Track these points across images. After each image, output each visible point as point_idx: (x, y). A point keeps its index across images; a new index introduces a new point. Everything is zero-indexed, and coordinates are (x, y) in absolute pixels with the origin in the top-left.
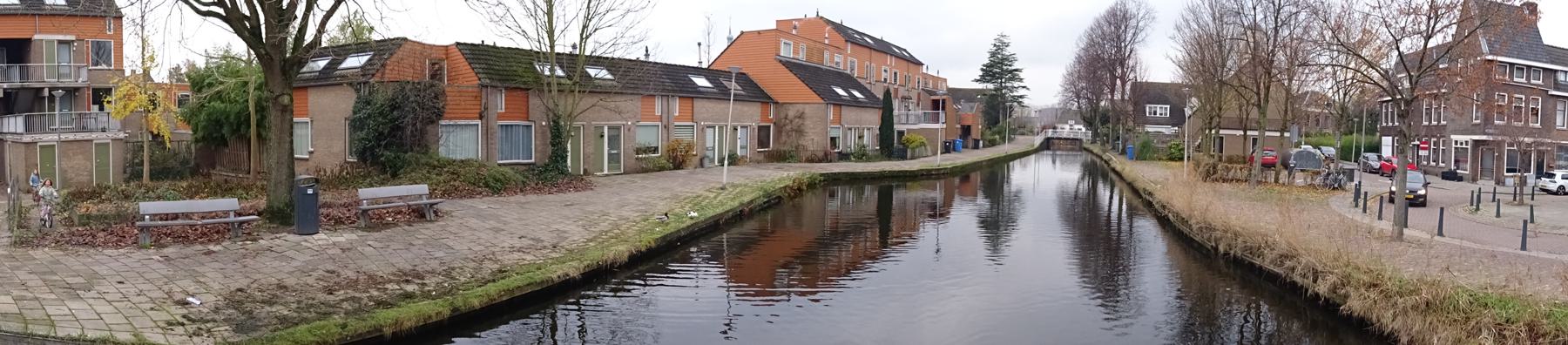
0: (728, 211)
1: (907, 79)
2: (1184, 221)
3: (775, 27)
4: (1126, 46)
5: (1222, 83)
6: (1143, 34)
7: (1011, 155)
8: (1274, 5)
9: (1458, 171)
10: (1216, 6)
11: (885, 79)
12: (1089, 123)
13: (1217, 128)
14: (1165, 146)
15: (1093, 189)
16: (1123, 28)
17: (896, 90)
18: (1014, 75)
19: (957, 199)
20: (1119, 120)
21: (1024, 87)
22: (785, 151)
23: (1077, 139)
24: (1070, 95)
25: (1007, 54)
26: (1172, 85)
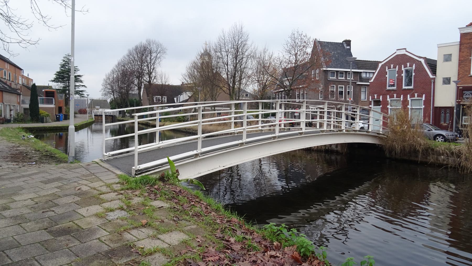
21: (83, 86)
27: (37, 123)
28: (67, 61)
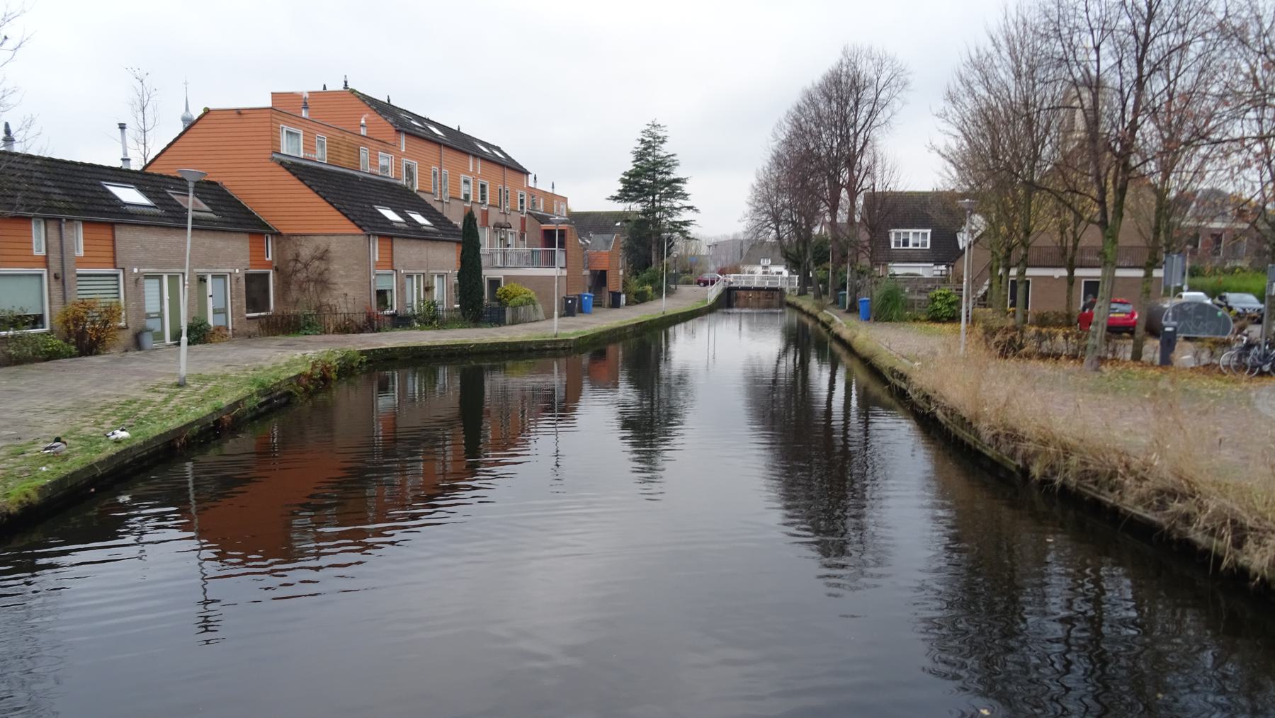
0: (191, 424)
1: (503, 195)
2: (965, 423)
3: (269, 104)
4: (856, 135)
5: (1031, 186)
6: (887, 111)
7: (671, 316)
8: (1137, 37)
10: (1022, 53)
11: (467, 197)
12: (794, 262)
13: (1021, 267)
14: (924, 297)
15: (802, 368)
16: (852, 103)
17: (485, 214)
18: (673, 188)
19: (586, 387)
20: (845, 256)
21: (689, 208)
22: (297, 317)
23: (776, 289)
24: (764, 217)
25: (662, 154)
26: (937, 196)
27: (476, 327)
28: (649, 141)
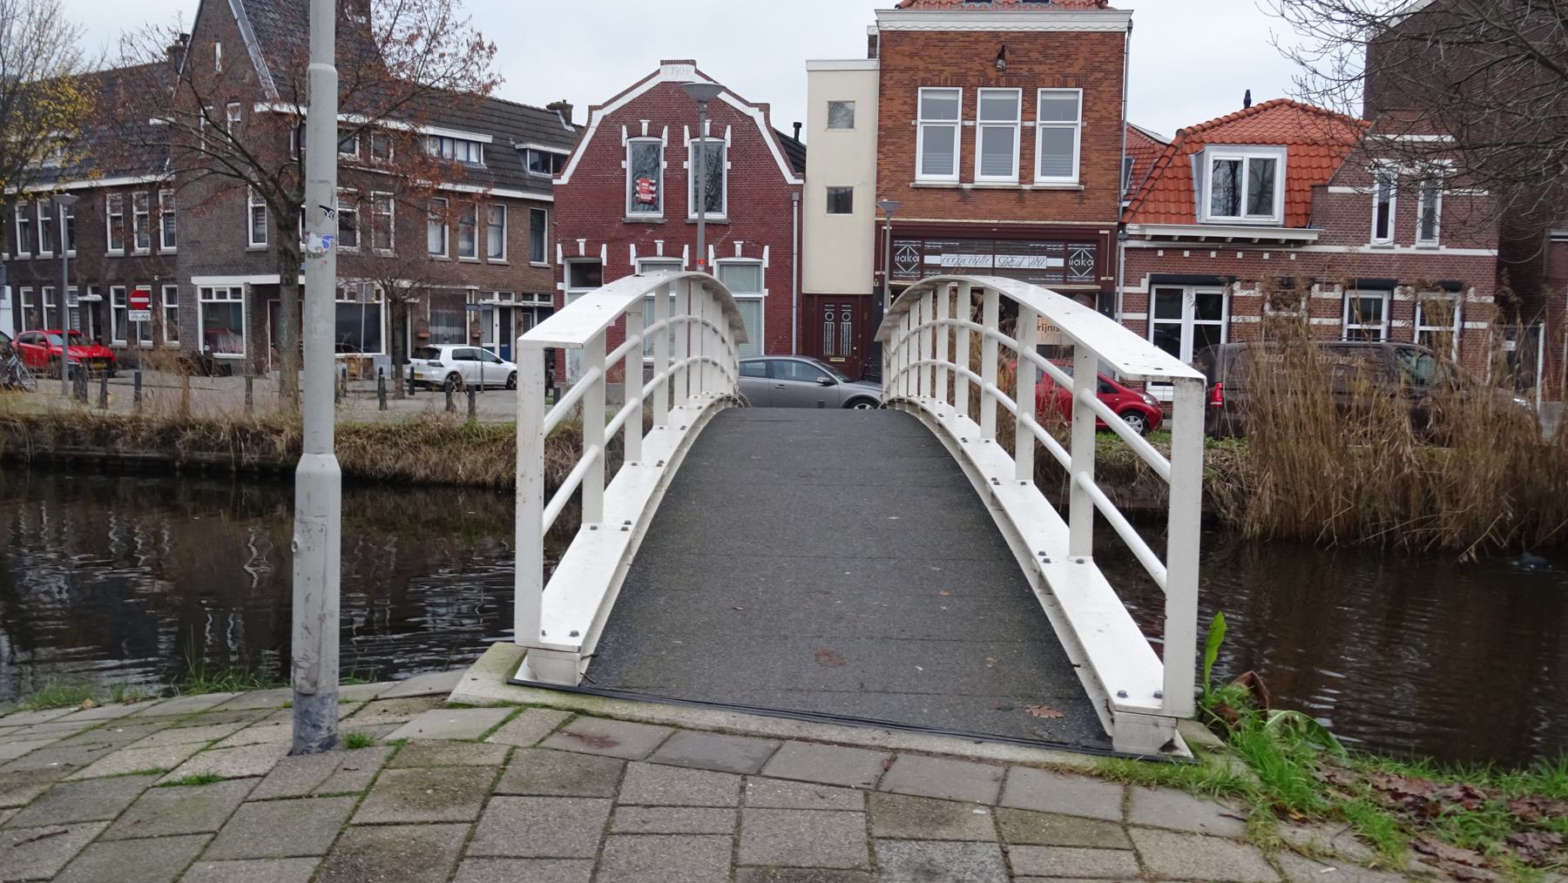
9: (217, 355)
